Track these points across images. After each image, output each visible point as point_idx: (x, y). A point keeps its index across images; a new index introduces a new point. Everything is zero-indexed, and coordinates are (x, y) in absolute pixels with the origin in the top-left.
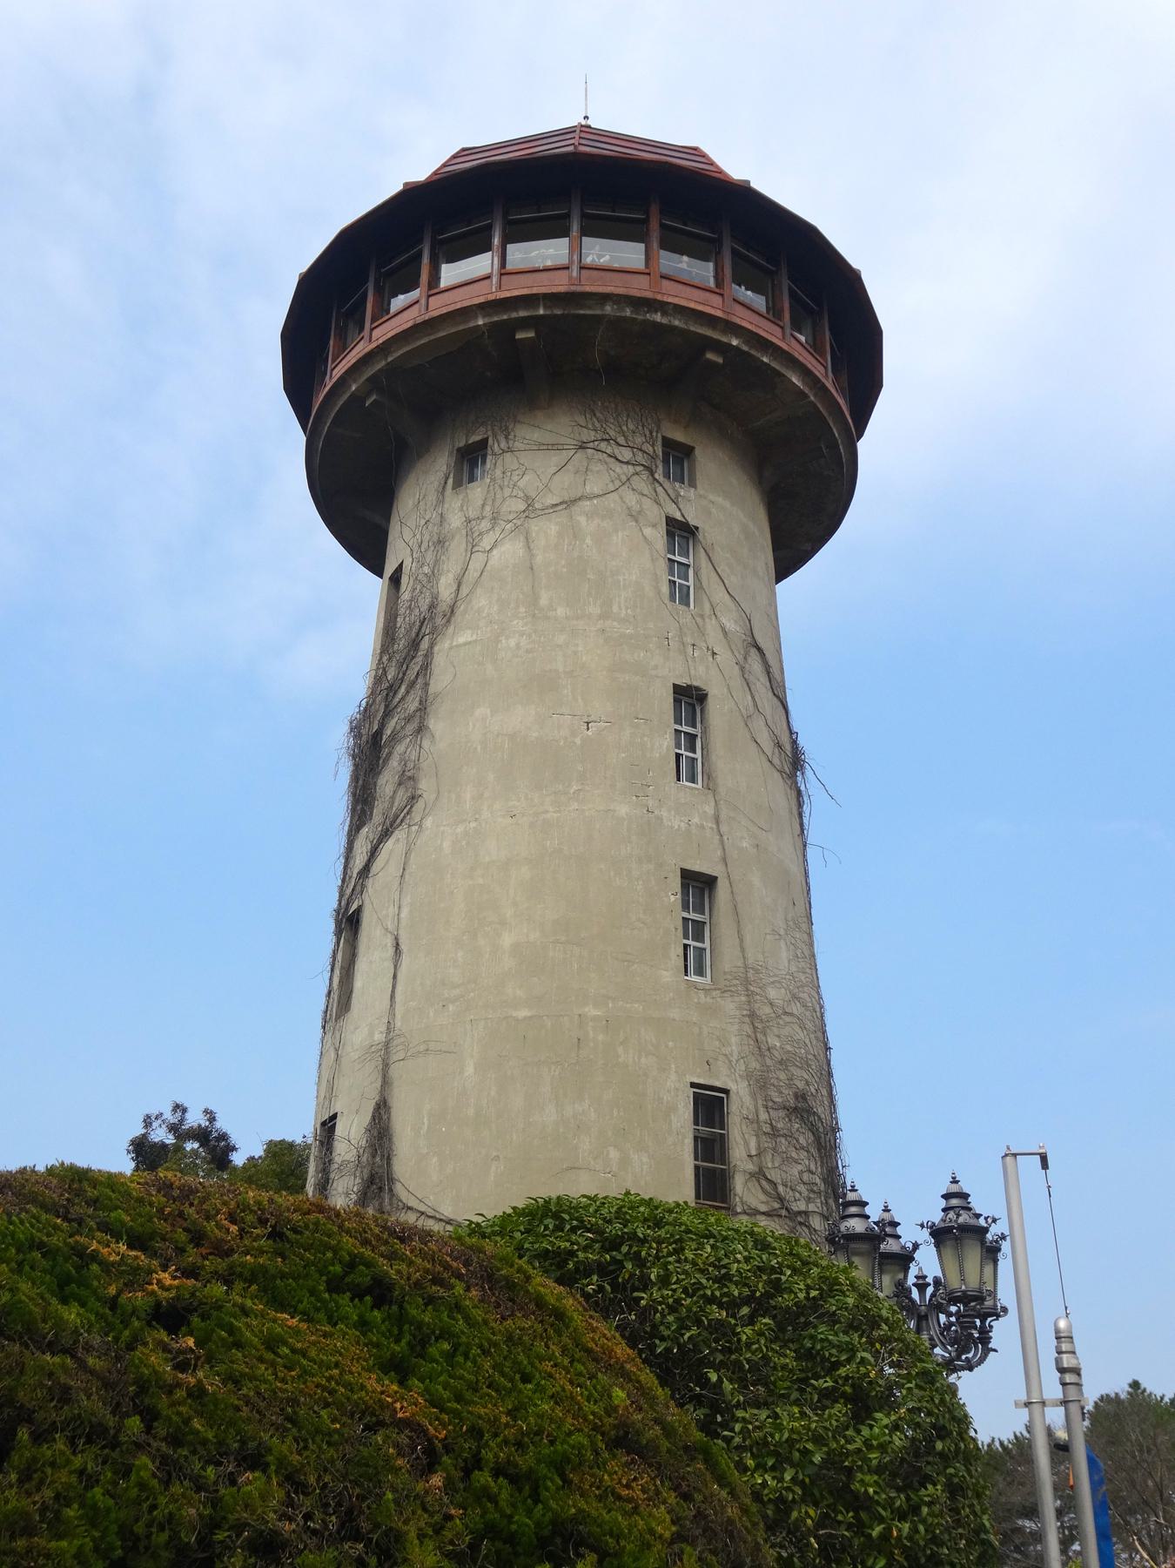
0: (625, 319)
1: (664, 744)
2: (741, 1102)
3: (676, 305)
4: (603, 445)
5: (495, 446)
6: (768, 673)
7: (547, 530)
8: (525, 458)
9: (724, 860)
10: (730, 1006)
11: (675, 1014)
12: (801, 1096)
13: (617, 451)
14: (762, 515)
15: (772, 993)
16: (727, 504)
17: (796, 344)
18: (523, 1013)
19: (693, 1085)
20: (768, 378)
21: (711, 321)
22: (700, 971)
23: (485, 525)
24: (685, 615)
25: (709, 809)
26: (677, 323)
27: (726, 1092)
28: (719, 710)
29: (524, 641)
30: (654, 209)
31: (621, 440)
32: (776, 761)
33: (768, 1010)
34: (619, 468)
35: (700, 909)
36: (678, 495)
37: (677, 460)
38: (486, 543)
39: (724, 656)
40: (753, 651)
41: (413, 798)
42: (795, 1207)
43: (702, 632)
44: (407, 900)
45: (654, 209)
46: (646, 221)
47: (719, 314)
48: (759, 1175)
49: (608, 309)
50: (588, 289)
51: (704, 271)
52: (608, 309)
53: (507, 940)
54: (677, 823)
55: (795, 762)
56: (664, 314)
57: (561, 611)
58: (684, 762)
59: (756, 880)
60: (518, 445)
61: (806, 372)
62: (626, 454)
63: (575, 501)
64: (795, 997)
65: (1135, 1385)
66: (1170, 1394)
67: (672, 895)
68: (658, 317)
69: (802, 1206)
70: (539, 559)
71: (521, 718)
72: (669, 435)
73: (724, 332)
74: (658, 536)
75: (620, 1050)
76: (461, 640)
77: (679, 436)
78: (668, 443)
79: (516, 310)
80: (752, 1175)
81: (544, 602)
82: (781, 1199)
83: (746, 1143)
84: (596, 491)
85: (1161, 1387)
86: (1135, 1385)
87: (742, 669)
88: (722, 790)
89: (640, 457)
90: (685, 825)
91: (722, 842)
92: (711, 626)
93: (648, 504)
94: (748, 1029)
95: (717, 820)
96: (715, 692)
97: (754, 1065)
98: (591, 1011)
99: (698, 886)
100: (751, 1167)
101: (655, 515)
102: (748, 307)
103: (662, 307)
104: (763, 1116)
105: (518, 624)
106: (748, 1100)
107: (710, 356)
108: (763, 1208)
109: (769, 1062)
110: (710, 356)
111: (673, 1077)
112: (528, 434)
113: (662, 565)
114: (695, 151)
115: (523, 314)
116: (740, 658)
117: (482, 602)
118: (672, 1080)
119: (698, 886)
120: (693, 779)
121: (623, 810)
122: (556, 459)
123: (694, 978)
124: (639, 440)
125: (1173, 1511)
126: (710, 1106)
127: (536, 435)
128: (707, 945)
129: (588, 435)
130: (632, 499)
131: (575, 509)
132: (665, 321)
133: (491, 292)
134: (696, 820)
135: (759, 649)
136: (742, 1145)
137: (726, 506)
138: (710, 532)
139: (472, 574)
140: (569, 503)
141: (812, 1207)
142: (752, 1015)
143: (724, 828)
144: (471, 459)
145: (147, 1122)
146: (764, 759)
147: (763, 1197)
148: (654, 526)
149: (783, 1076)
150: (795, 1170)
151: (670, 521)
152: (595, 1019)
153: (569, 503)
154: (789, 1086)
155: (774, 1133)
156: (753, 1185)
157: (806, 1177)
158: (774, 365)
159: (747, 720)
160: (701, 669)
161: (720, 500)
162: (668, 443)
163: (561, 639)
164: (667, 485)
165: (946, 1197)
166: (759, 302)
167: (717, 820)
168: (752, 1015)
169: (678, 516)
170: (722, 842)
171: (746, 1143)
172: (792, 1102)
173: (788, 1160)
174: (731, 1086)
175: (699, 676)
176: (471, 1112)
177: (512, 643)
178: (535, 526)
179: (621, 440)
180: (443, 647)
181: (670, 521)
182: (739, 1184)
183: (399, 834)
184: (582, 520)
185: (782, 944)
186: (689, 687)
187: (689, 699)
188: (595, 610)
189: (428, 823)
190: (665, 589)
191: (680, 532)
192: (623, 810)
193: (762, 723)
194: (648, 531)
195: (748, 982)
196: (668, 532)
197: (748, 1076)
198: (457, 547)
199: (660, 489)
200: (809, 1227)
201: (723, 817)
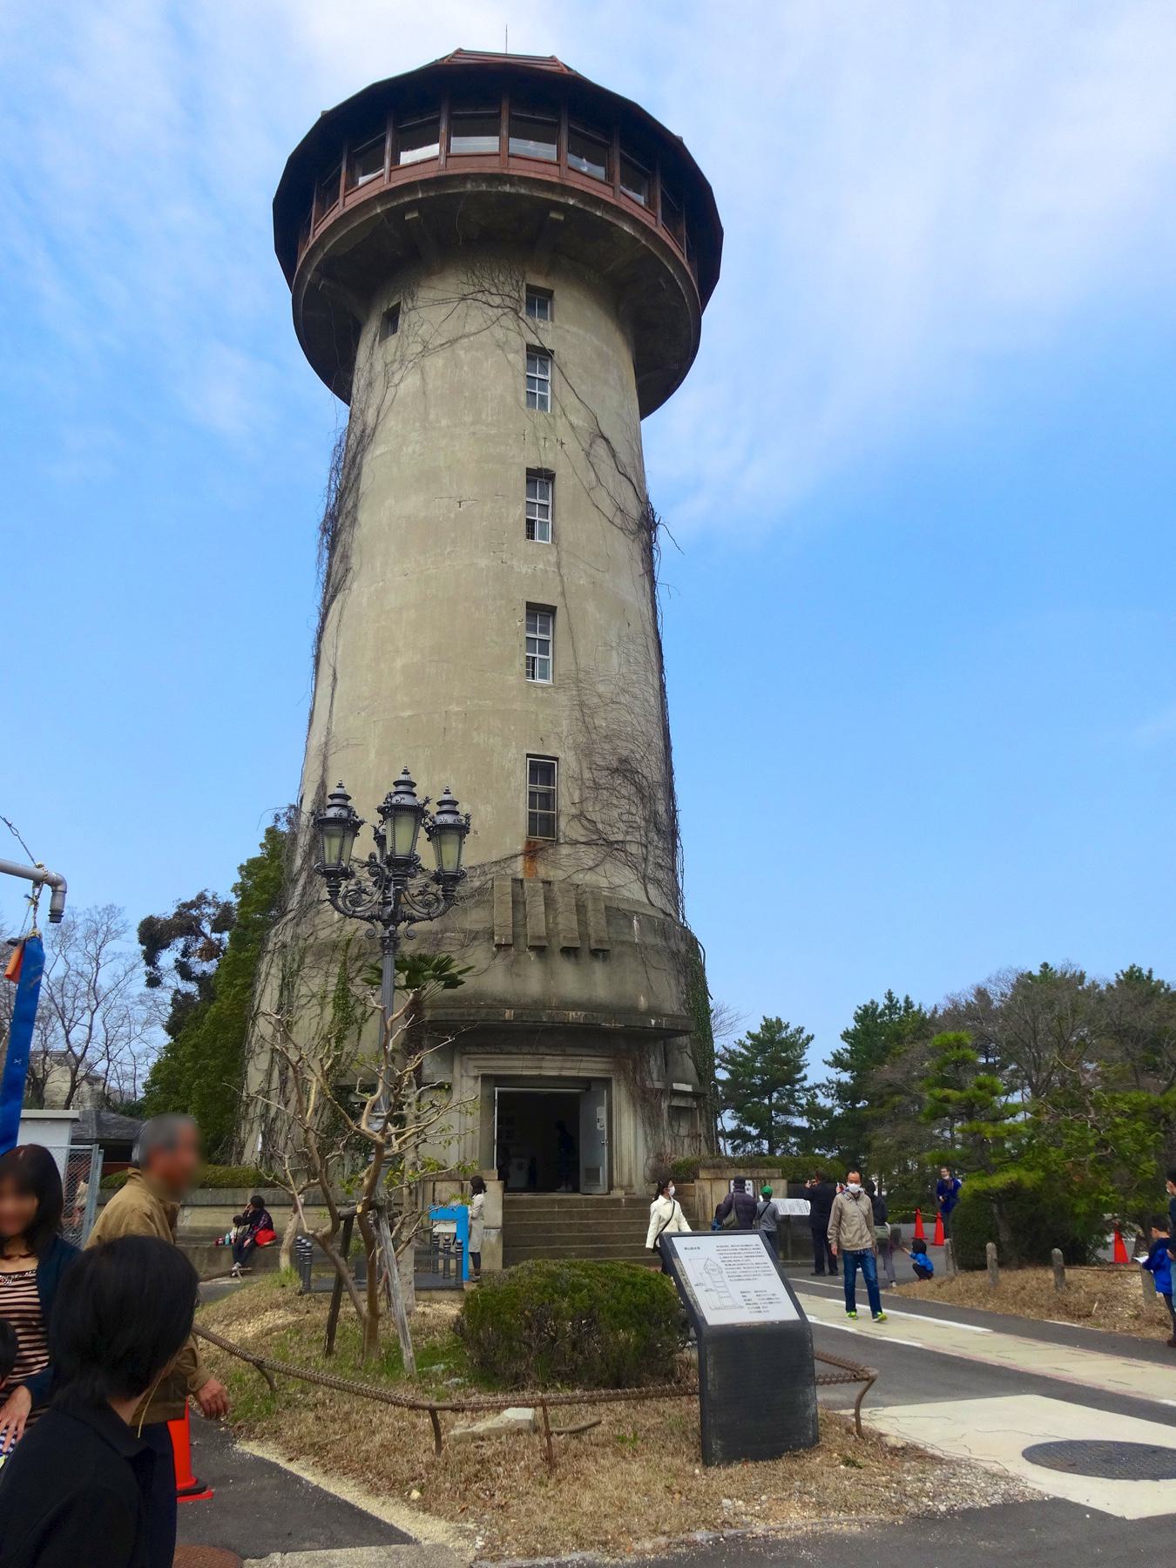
0: (481, 193)
1: (517, 514)
2: (569, 765)
3: (520, 177)
4: (479, 296)
5: (404, 307)
6: (614, 456)
7: (436, 363)
8: (424, 313)
9: (563, 594)
10: (563, 699)
11: (517, 706)
12: (624, 761)
13: (490, 299)
14: (618, 339)
15: (601, 688)
16: (582, 332)
17: (634, 201)
18: (408, 713)
19: (528, 756)
20: (606, 230)
21: (549, 186)
22: (543, 676)
23: (396, 365)
24: (539, 417)
25: (553, 558)
26: (523, 191)
27: (556, 759)
28: (565, 484)
29: (418, 447)
30: (505, 105)
31: (494, 290)
32: (618, 521)
33: (596, 700)
34: (490, 312)
35: (544, 630)
36: (537, 327)
37: (539, 301)
38: (396, 379)
39: (572, 445)
40: (600, 441)
41: (347, 570)
42: (612, 838)
43: (552, 428)
44: (341, 643)
45: (505, 105)
46: (499, 116)
47: (555, 180)
48: (581, 816)
49: (469, 187)
50: (451, 172)
51: (547, 151)
52: (469, 187)
53: (399, 663)
54: (525, 569)
55: (647, 524)
56: (512, 185)
57: (444, 423)
58: (537, 526)
59: (591, 607)
60: (420, 304)
61: (634, 221)
62: (497, 300)
63: (456, 340)
64: (623, 690)
65: (1045, 965)
66: (1170, 979)
67: (519, 620)
68: (507, 188)
69: (620, 837)
70: (430, 386)
71: (414, 504)
72: (532, 283)
73: (562, 195)
74: (519, 360)
75: (475, 734)
76: (378, 452)
77: (540, 282)
78: (530, 289)
79: (402, 196)
80: (574, 816)
81: (432, 417)
82: (598, 831)
83: (571, 795)
84: (473, 330)
85: (1164, 974)
86: (1045, 965)
87: (588, 455)
88: (564, 544)
89: (508, 302)
90: (533, 570)
91: (562, 582)
92: (561, 424)
93: (512, 335)
94: (577, 714)
95: (559, 565)
96: (562, 473)
97: (581, 739)
98: (455, 708)
99: (540, 613)
100: (574, 811)
101: (518, 343)
102: (586, 174)
103: (510, 179)
104: (587, 775)
105: (414, 436)
106: (574, 765)
107: (553, 215)
108: (583, 839)
109: (594, 737)
110: (553, 215)
111: (513, 750)
112: (425, 294)
113: (522, 381)
114: (553, 59)
115: (407, 199)
116: (586, 446)
117: (392, 424)
118: (512, 753)
119: (540, 613)
120: (544, 537)
121: (483, 562)
122: (445, 310)
123: (538, 681)
124: (507, 289)
125: (1174, 1054)
126: (542, 769)
127: (432, 294)
128: (550, 657)
129: (467, 289)
130: (499, 333)
131: (457, 345)
132: (513, 191)
133: (493, 167)
134: (541, 566)
135: (606, 440)
136: (566, 795)
137: (585, 337)
138: (563, 353)
139: (387, 403)
140: (452, 342)
141: (629, 838)
142: (582, 705)
143: (564, 571)
144: (391, 321)
145: (277, 818)
146: (605, 520)
147: (583, 832)
148: (517, 352)
149: (607, 746)
150: (615, 813)
151: (530, 348)
152: (457, 714)
153: (452, 342)
154: (614, 754)
155: (597, 787)
156: (576, 824)
157: (625, 817)
158: (607, 217)
159: (589, 491)
160: (551, 456)
161: (575, 329)
162: (530, 289)
163: (443, 442)
164: (529, 321)
165: (397, 784)
166: (600, 172)
167: (559, 565)
168: (582, 705)
169: (537, 343)
170: (562, 582)
171: (571, 795)
172: (615, 764)
173: (609, 805)
174: (560, 755)
175: (547, 460)
176: (372, 785)
177: (410, 449)
178: (428, 362)
179: (494, 290)
180: (368, 458)
181: (530, 348)
182: (563, 823)
183: (339, 597)
184: (462, 353)
185: (614, 653)
186: (540, 470)
187: (539, 478)
188: (468, 419)
189: (355, 586)
190: (523, 398)
191: (538, 355)
192: (483, 562)
193: (604, 493)
194: (511, 356)
195: (578, 681)
196: (529, 357)
197: (576, 747)
198: (379, 385)
199: (523, 325)
200: (625, 851)
201: (563, 563)
